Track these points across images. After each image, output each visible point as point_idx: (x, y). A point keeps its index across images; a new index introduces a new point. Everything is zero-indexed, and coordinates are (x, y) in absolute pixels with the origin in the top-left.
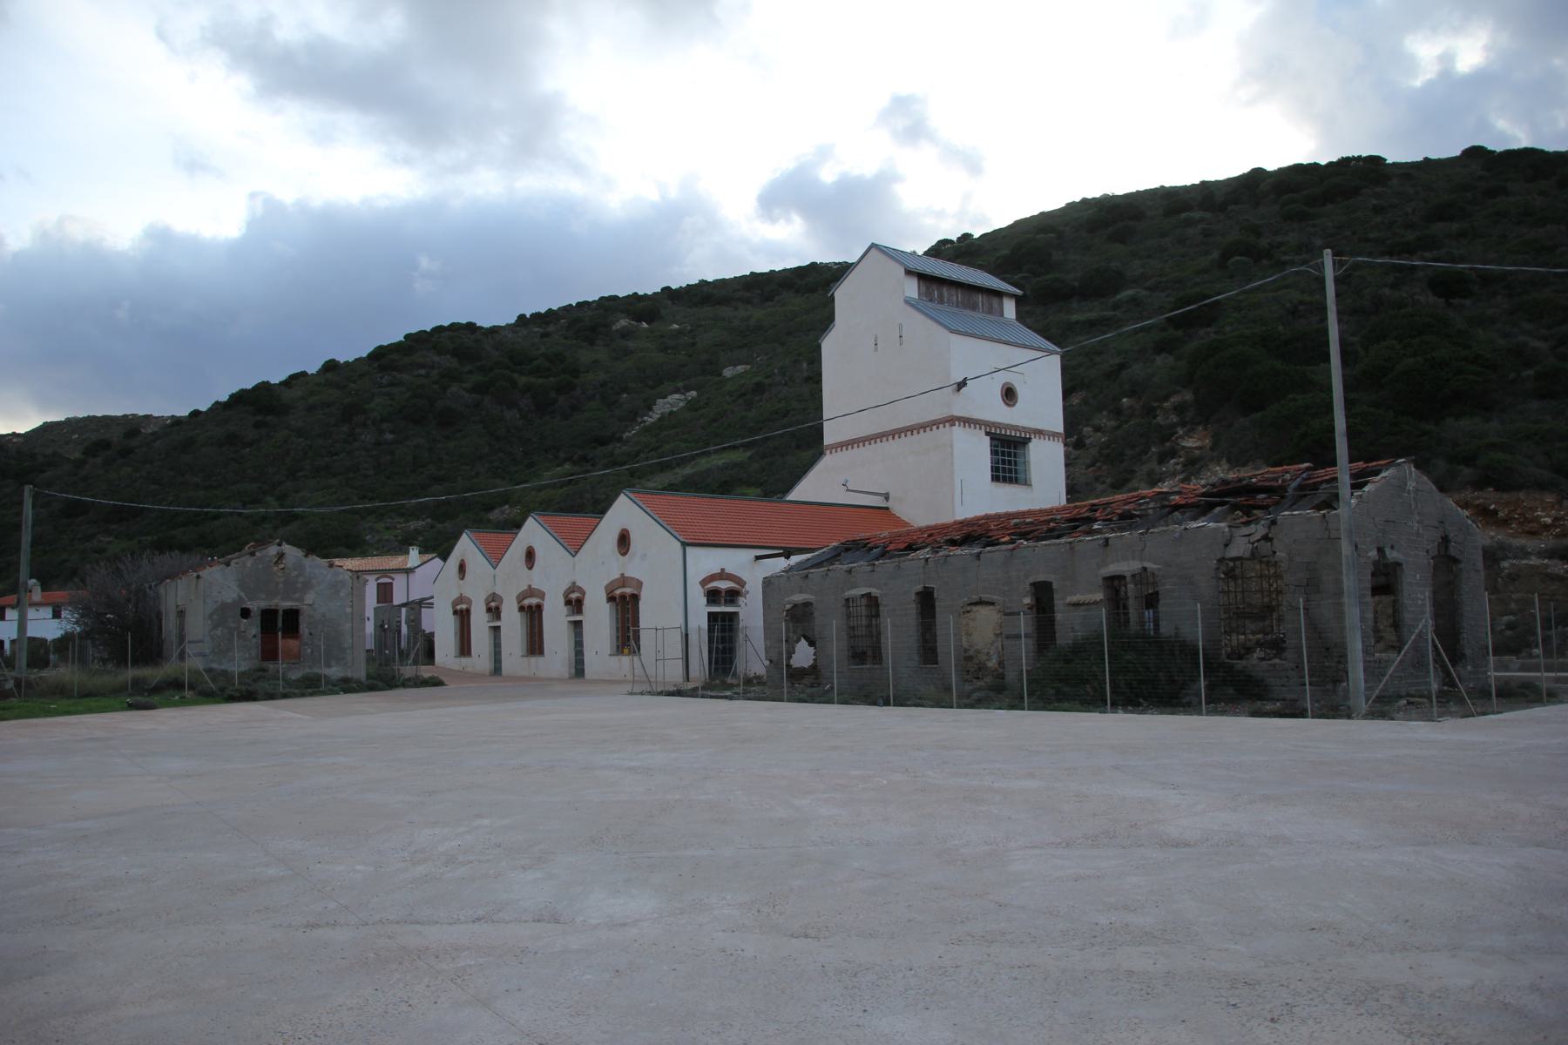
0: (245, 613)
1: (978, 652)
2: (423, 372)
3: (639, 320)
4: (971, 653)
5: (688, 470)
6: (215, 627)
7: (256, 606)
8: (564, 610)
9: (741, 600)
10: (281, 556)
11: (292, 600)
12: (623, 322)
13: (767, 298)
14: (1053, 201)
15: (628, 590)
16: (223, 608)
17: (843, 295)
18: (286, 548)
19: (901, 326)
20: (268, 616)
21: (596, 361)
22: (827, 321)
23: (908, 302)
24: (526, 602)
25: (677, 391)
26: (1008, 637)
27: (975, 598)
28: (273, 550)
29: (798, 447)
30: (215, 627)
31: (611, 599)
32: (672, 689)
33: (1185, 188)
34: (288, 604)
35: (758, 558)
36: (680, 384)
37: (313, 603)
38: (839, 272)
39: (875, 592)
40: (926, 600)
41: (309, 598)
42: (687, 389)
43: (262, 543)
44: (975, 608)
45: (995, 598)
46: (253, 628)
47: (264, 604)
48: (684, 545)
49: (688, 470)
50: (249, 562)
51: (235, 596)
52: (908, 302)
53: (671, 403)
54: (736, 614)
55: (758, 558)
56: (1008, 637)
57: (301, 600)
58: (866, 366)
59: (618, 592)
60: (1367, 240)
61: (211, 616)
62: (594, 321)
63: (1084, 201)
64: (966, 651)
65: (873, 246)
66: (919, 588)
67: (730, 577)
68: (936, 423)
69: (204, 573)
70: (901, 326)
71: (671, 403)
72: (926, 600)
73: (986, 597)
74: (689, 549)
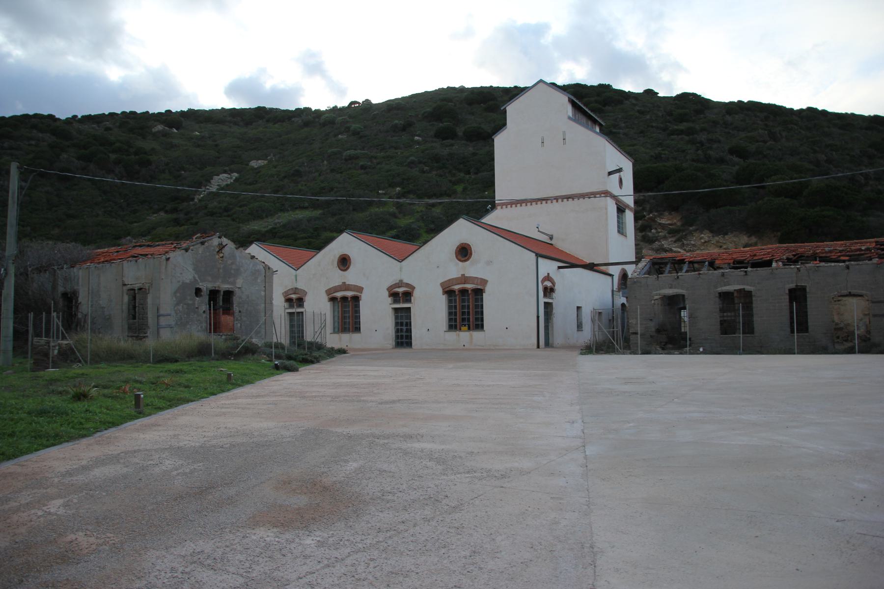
0: (198, 292)
1: (848, 325)
2: (33, 142)
3: (171, 127)
4: (842, 325)
5: (283, 218)
6: (178, 304)
7: (206, 286)
8: (390, 300)
9: (554, 295)
10: (222, 247)
11: (229, 283)
12: (160, 127)
13: (248, 123)
14: (431, 87)
15: (349, 294)
16: (184, 286)
17: (513, 110)
18: (225, 241)
19: (564, 133)
20: (213, 294)
21: (153, 149)
22: (501, 125)
23: (569, 118)
24: (339, 295)
25: (225, 172)
26: (875, 316)
27: (845, 292)
28: (215, 241)
29: (354, 210)
30: (178, 304)
31: (333, 299)
32: (338, 358)
33: (403, 98)
34: (225, 287)
35: (559, 268)
36: (227, 168)
37: (243, 287)
38: (514, 93)
39: (748, 288)
40: (797, 295)
41: (240, 282)
42: (232, 171)
43: (206, 233)
44: (844, 299)
45: (864, 292)
46: (202, 303)
47: (210, 286)
48: (538, 255)
49: (283, 218)
50: (201, 249)
51: (191, 277)
52: (569, 118)
53: (222, 180)
54: (409, 309)
55: (559, 268)
56: (875, 316)
57: (234, 283)
58: (517, 158)
59: (457, 287)
60: (652, 127)
61: (175, 293)
62: (136, 123)
63: (223, 109)
64: (837, 324)
65: (541, 81)
66: (793, 286)
67: (407, 285)
68: (593, 195)
69: (171, 255)
70: (564, 133)
71: (222, 180)
72: (797, 295)
73: (854, 291)
74: (540, 259)
